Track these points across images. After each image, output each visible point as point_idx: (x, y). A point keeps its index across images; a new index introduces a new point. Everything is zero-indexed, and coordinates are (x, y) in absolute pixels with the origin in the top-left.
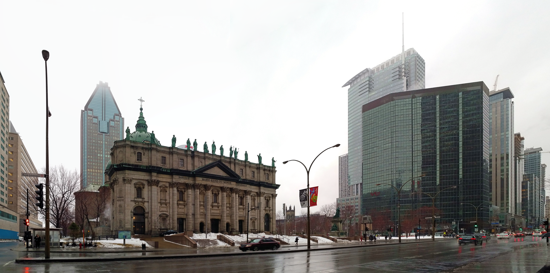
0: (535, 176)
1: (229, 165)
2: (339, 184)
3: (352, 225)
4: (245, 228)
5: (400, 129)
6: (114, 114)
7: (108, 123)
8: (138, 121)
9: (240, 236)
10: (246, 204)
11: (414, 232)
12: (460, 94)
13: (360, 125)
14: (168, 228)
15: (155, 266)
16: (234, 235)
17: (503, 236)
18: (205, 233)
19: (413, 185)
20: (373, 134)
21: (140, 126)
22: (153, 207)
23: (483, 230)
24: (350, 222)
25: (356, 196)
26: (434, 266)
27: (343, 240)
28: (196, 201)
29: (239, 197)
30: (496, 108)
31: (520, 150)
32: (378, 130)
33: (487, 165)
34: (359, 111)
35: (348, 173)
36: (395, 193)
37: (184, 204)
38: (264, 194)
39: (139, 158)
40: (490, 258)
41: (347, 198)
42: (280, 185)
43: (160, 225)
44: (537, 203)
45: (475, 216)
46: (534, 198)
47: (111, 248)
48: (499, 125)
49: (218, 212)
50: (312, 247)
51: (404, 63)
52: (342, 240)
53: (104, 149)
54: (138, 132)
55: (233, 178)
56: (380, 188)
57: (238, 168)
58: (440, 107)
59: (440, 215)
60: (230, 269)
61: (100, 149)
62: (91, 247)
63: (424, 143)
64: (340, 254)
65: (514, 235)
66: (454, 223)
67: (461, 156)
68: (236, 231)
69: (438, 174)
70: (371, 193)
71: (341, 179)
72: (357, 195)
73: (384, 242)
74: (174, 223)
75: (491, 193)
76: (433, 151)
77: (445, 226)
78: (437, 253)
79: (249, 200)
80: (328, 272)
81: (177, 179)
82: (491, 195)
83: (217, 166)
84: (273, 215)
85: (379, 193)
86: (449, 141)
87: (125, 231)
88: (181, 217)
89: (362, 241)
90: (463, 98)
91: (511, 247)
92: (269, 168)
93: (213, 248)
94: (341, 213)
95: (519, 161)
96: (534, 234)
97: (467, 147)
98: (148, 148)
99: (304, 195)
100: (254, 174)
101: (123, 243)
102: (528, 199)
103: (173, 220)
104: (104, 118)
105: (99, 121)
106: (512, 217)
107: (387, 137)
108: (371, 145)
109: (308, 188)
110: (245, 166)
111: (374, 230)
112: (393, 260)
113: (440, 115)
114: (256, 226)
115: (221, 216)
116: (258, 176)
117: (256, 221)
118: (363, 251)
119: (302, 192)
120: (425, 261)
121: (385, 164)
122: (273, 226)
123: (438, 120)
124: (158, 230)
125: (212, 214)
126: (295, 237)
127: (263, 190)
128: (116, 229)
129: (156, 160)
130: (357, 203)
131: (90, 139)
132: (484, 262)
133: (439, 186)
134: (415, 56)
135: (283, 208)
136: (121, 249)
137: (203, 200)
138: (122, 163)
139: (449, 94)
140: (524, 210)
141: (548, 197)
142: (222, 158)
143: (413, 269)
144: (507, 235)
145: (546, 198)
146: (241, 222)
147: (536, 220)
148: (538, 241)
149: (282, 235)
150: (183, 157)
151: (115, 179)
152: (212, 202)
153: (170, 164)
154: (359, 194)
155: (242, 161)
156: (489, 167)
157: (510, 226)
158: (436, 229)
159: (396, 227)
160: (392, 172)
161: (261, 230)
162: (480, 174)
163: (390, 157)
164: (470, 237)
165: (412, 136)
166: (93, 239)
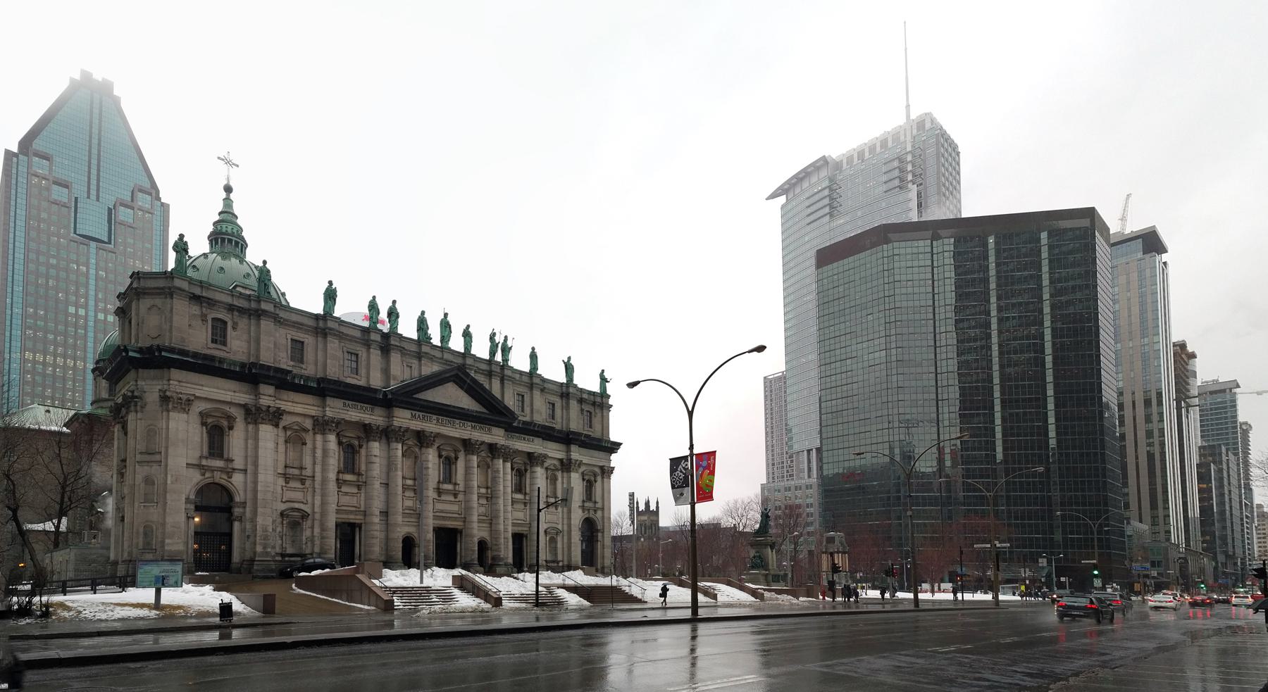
0: (1227, 450)
1: (488, 381)
2: (767, 446)
3: (801, 557)
4: (529, 557)
5: (905, 317)
6: (132, 185)
7: (110, 210)
8: (215, 224)
9: (517, 579)
10: (531, 490)
11: (950, 582)
12: (1044, 235)
13: (811, 298)
14: (307, 552)
15: (261, 670)
16: (500, 576)
17: (1162, 602)
18: (418, 569)
19: (941, 460)
20: (842, 326)
21: (223, 240)
22: (259, 488)
23: (1114, 585)
24: (795, 549)
25: (805, 480)
26: (1003, 675)
27: (779, 596)
28: (392, 474)
29: (512, 469)
30: (1128, 275)
31: (1188, 384)
32: (853, 315)
33: (1112, 416)
34: (808, 263)
35: (786, 420)
36: (899, 478)
37: (359, 481)
38: (579, 466)
39: (219, 333)
40: (1135, 660)
41: (786, 484)
42: (621, 444)
43: (280, 542)
44: (1236, 521)
45: (1093, 548)
46: (1227, 508)
47: (106, 620)
48: (1136, 319)
49: (455, 508)
50: (702, 613)
51: (910, 149)
52: (776, 595)
53: (92, 293)
54: (215, 255)
55: (497, 418)
56: (863, 462)
57: (512, 391)
58: (998, 265)
59: (1010, 540)
60: (488, 674)
61: (77, 289)
62: (28, 621)
63: (962, 354)
64: (773, 632)
65: (1187, 602)
66: (1043, 562)
67: (1050, 392)
68: (506, 565)
69: (999, 435)
70: (843, 474)
71: (770, 435)
72: (809, 477)
73: (879, 604)
74: (327, 538)
75: (1126, 490)
76: (985, 376)
77: (1022, 570)
78: (1008, 640)
79: (539, 477)
80: (744, 682)
81: (336, 409)
82: (1127, 494)
83: (454, 382)
84: (603, 523)
85: (863, 473)
86: (1022, 352)
87: (162, 560)
88: (347, 521)
89: (824, 599)
90: (1051, 247)
91: (1183, 631)
92: (592, 397)
93: (441, 613)
94: (772, 523)
95: (1188, 412)
96: (1234, 600)
97: (1064, 370)
98: (249, 310)
99: (681, 471)
100: (553, 410)
101: (152, 600)
102: (1213, 508)
103: (323, 529)
104: (93, 192)
105: (76, 199)
106: (1179, 552)
107: (877, 335)
108: (838, 352)
109: (692, 454)
110: (531, 386)
111: (853, 572)
112: (902, 655)
113: (997, 286)
114: (560, 552)
115: (464, 522)
116: (565, 417)
117: (559, 539)
118: (829, 628)
119: (675, 463)
120: (979, 661)
121: (873, 401)
122: (606, 554)
123: (993, 299)
124: (274, 556)
125: (437, 514)
126: (660, 584)
127: (577, 454)
128: (130, 554)
129: (273, 346)
130: (808, 495)
131: (38, 253)
132: (1121, 670)
133: (1002, 466)
134: (936, 132)
135: (630, 503)
136: (146, 623)
137: (412, 474)
138: (158, 346)
139: (1018, 235)
140: (1208, 538)
141: (1260, 506)
142: (469, 361)
143: (951, 681)
144: (1172, 599)
145: (1255, 509)
146: (518, 539)
147: (1236, 564)
148: (1245, 619)
149: (625, 578)
150: (358, 349)
151: (133, 392)
152: (439, 480)
153: (316, 364)
154: (815, 476)
155: (521, 373)
156: (1117, 424)
157: (1178, 578)
158: (1001, 576)
159: (907, 567)
160: (889, 423)
161: (573, 563)
162: (1096, 438)
163: (884, 386)
164: (1082, 602)
165: (935, 336)
166: (38, 592)
